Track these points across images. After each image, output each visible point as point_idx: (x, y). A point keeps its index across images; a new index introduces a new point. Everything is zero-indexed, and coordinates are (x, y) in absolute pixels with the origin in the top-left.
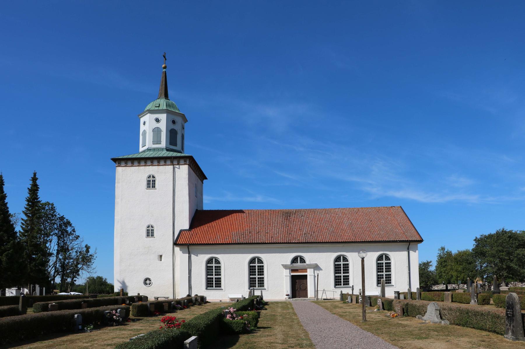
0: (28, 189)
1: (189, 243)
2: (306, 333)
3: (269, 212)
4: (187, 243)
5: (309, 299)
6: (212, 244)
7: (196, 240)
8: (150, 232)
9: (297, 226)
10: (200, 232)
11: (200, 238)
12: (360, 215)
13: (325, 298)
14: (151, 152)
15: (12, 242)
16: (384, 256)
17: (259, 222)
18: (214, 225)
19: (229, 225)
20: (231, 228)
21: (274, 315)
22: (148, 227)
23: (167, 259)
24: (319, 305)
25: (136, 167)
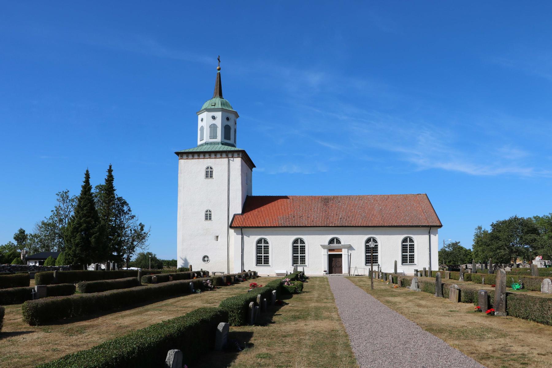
0: (105, 179)
1: (242, 226)
2: (332, 294)
3: (310, 198)
4: (241, 226)
5: (343, 275)
6: (262, 227)
7: (248, 223)
8: (208, 216)
9: (334, 211)
10: (251, 216)
11: (251, 222)
12: (389, 201)
13: (357, 274)
14: (209, 146)
15: (98, 226)
16: (408, 239)
17: (302, 207)
18: (262, 210)
19: (276, 210)
20: (277, 212)
21: (313, 286)
22: (206, 212)
23: (223, 239)
24: (349, 279)
25: (196, 160)
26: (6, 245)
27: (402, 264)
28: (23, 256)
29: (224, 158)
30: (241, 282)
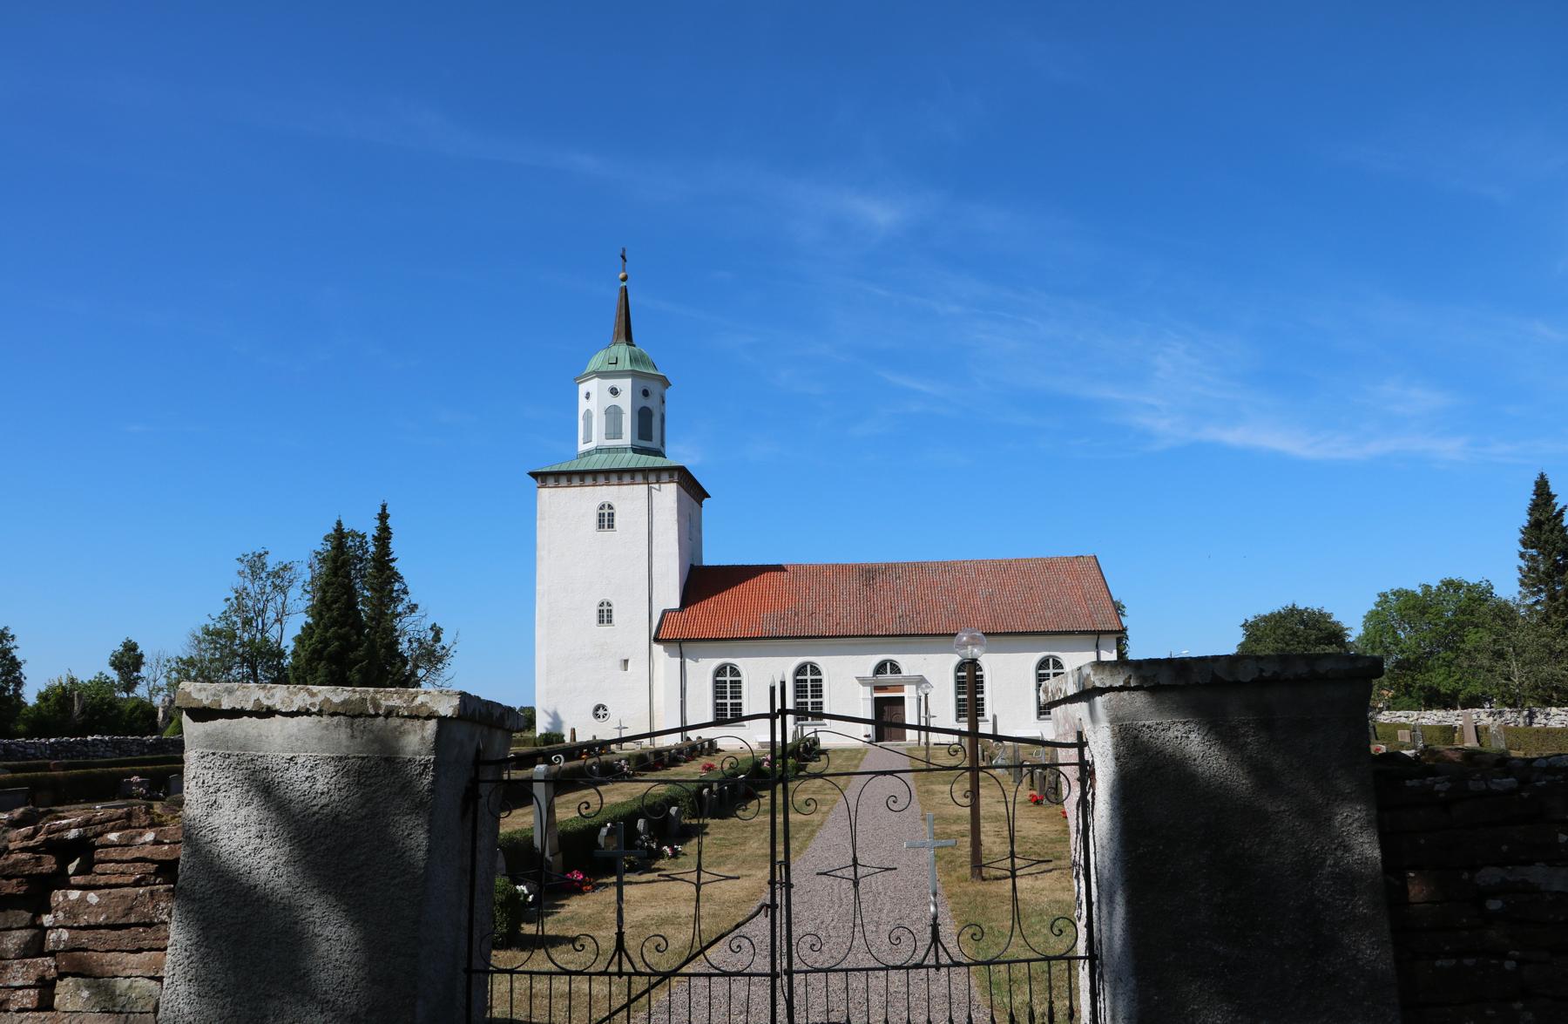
0: (373, 536)
6: (726, 639)
14: (604, 456)
16: (1051, 660)
23: (638, 667)
26: (90, 681)
27: (1038, 718)
28: (163, 711)
29: (638, 484)
30: (682, 764)
